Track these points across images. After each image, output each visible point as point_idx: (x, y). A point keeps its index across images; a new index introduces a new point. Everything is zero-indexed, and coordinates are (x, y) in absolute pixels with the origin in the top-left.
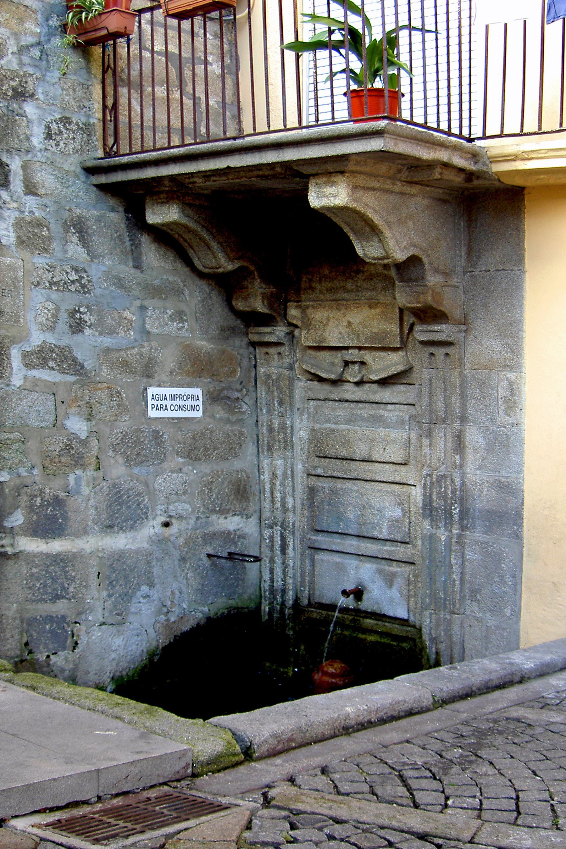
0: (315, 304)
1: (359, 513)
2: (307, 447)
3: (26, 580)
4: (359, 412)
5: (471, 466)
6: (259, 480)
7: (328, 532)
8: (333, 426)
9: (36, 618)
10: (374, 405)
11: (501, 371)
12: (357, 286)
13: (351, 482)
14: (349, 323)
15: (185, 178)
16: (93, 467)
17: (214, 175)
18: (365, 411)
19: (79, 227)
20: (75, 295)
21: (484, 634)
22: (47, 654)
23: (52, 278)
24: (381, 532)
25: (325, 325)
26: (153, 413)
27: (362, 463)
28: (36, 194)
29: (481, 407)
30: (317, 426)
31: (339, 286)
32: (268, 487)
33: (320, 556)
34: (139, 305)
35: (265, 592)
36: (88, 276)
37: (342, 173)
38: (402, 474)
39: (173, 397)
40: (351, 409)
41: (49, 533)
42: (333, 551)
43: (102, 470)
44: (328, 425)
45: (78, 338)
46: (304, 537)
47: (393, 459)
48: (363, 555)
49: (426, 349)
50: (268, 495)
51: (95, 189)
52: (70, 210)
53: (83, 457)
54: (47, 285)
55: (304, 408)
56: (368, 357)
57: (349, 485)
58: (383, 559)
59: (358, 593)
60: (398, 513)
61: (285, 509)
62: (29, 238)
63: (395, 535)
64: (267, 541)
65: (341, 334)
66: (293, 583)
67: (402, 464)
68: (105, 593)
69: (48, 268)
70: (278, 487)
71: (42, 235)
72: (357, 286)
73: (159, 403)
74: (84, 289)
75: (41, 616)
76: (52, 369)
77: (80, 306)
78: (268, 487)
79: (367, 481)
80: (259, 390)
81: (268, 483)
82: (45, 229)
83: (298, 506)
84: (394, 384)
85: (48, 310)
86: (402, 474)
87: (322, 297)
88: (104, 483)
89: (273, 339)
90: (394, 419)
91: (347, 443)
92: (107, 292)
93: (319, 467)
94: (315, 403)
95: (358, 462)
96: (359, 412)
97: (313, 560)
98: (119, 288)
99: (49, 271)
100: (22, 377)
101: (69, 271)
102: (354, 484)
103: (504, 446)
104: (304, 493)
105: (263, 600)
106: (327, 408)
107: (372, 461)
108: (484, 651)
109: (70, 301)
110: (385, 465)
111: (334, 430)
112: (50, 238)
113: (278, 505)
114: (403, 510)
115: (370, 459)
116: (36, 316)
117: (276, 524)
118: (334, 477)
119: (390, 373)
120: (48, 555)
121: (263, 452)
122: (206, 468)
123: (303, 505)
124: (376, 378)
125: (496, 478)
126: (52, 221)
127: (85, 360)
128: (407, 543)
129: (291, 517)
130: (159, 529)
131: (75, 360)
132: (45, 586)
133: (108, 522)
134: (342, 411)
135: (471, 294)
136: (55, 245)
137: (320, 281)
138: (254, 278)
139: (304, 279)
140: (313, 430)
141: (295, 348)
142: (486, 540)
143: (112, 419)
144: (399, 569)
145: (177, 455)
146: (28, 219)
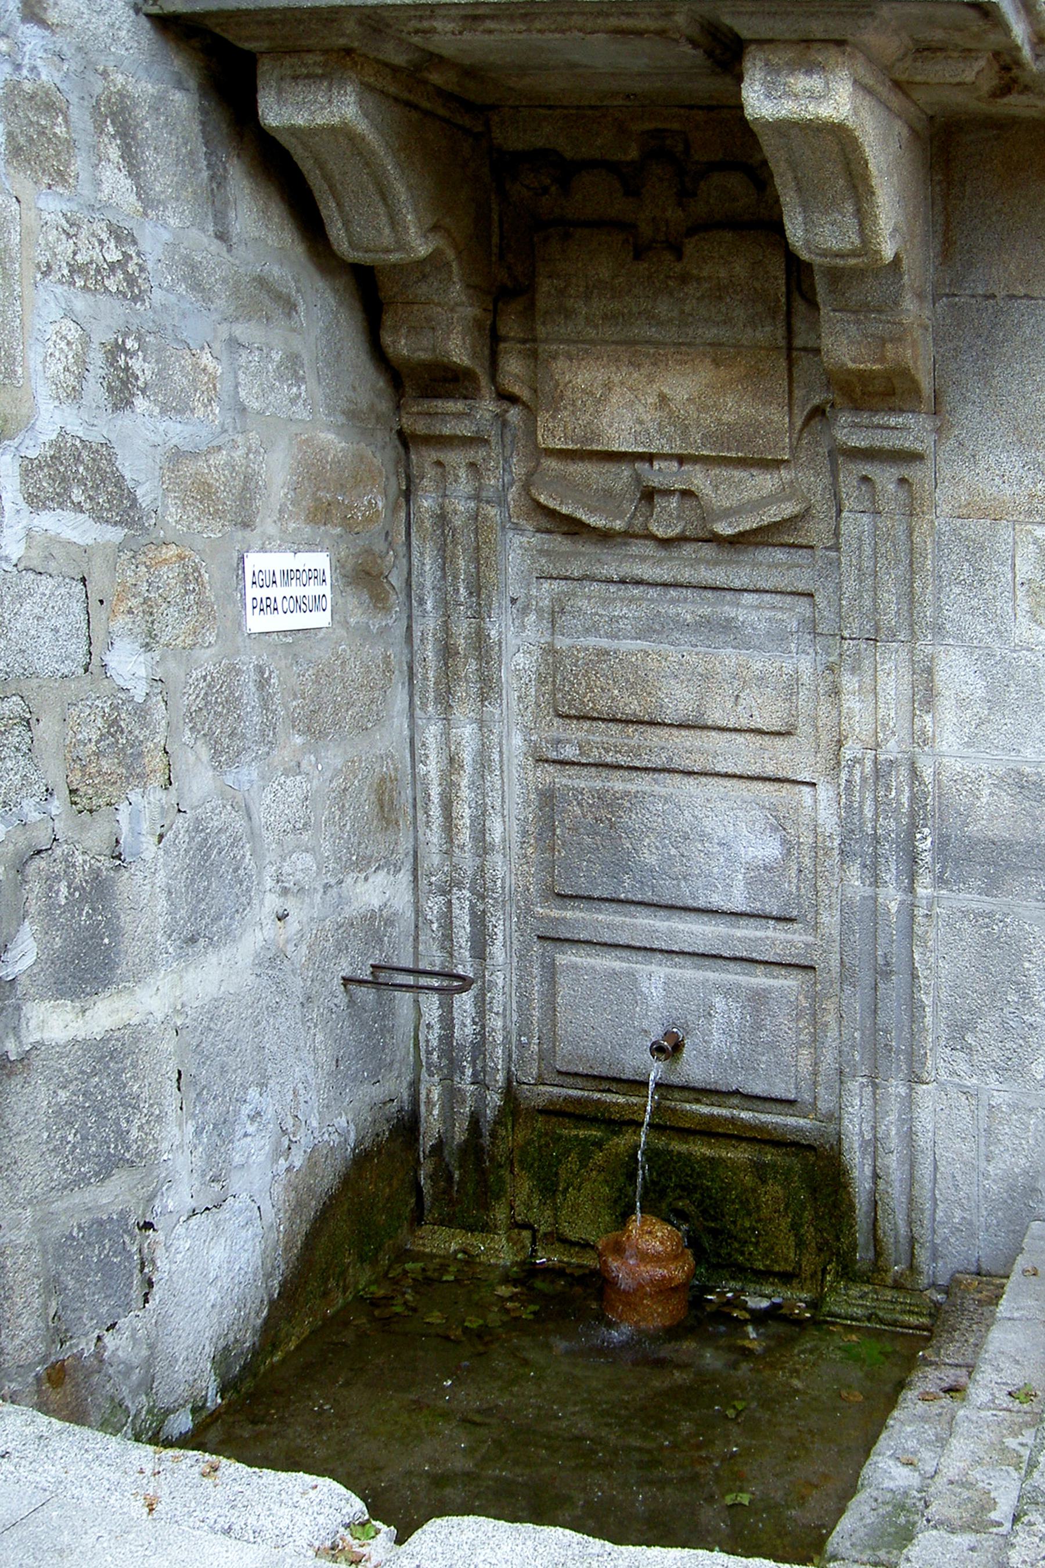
0: (573, 350)
1: (673, 851)
2: (533, 691)
3: (48, 1129)
4: (672, 610)
5: (952, 738)
6: (414, 775)
7: (590, 898)
8: (604, 643)
9: (71, 1237)
10: (709, 594)
11: (1020, 523)
12: (682, 312)
13: (648, 777)
14: (663, 399)
15: (410, 19)
16: (157, 780)
17: (493, 17)
18: (689, 608)
19: (118, 117)
20: (117, 303)
21: (983, 1125)
22: (95, 1335)
23: (75, 253)
24: (729, 895)
25: (599, 401)
26: (257, 622)
27: (675, 731)
28: (42, 23)
29: (974, 602)
30: (562, 643)
31: (635, 310)
32: (435, 792)
33: (566, 958)
34: (226, 336)
35: (429, 1053)
36: (138, 254)
37: (840, 43)
38: (777, 756)
39: (289, 576)
40: (652, 600)
41: (87, 982)
42: (605, 944)
43: (175, 785)
44: (592, 641)
45: (125, 420)
46: (528, 910)
47: (758, 723)
48: (682, 953)
49: (852, 466)
50: (435, 811)
51: (147, 24)
52: (105, 74)
53: (141, 754)
54: (66, 272)
55: (528, 596)
56: (699, 479)
57: (641, 784)
58: (735, 959)
59: (669, 1049)
60: (770, 849)
61: (483, 847)
62: (30, 140)
63: (763, 903)
64: (435, 926)
65: (641, 423)
66: (504, 1028)
67: (779, 734)
68: (190, 1128)
69: (66, 226)
70: (465, 793)
71: (55, 134)
72: (682, 312)
73: (264, 593)
74: (134, 291)
75: (80, 1228)
76: (78, 508)
77: (126, 335)
78: (435, 792)
79: (690, 773)
80: (415, 553)
81: (436, 782)
82: (60, 119)
83: (516, 837)
84: (757, 545)
85: (69, 343)
86: (777, 756)
87: (592, 333)
88: (180, 818)
89: (465, 429)
90: (763, 626)
91: (639, 682)
92: (173, 299)
93: (569, 741)
94: (555, 585)
95: (667, 730)
96: (672, 610)
97: (551, 972)
98: (193, 289)
99: (69, 236)
100: (22, 533)
101: (104, 236)
102: (656, 781)
103: (1030, 693)
104: (527, 803)
105: (424, 1075)
106: (589, 598)
107: (705, 727)
108: (983, 1164)
109: (107, 317)
110: (734, 735)
111: (608, 653)
112: (70, 144)
113: (465, 837)
114: (784, 841)
115: (701, 723)
116: (45, 360)
117: (460, 886)
118: (606, 766)
119: (766, 520)
120: (85, 1045)
121: (424, 706)
122: (334, 757)
123: (525, 833)
124: (729, 531)
125: (1012, 765)
126: (74, 99)
127: (138, 483)
128: (791, 920)
129: (498, 866)
130: (270, 930)
131: (119, 480)
132: (84, 1138)
133: (188, 930)
134: (629, 608)
135: (950, 345)
136: (79, 165)
137: (587, 297)
138: (450, 279)
139: (545, 289)
140: (550, 650)
141: (507, 453)
142: (988, 908)
143: (189, 641)
144: (771, 982)
145: (294, 727)
146: (27, 86)
